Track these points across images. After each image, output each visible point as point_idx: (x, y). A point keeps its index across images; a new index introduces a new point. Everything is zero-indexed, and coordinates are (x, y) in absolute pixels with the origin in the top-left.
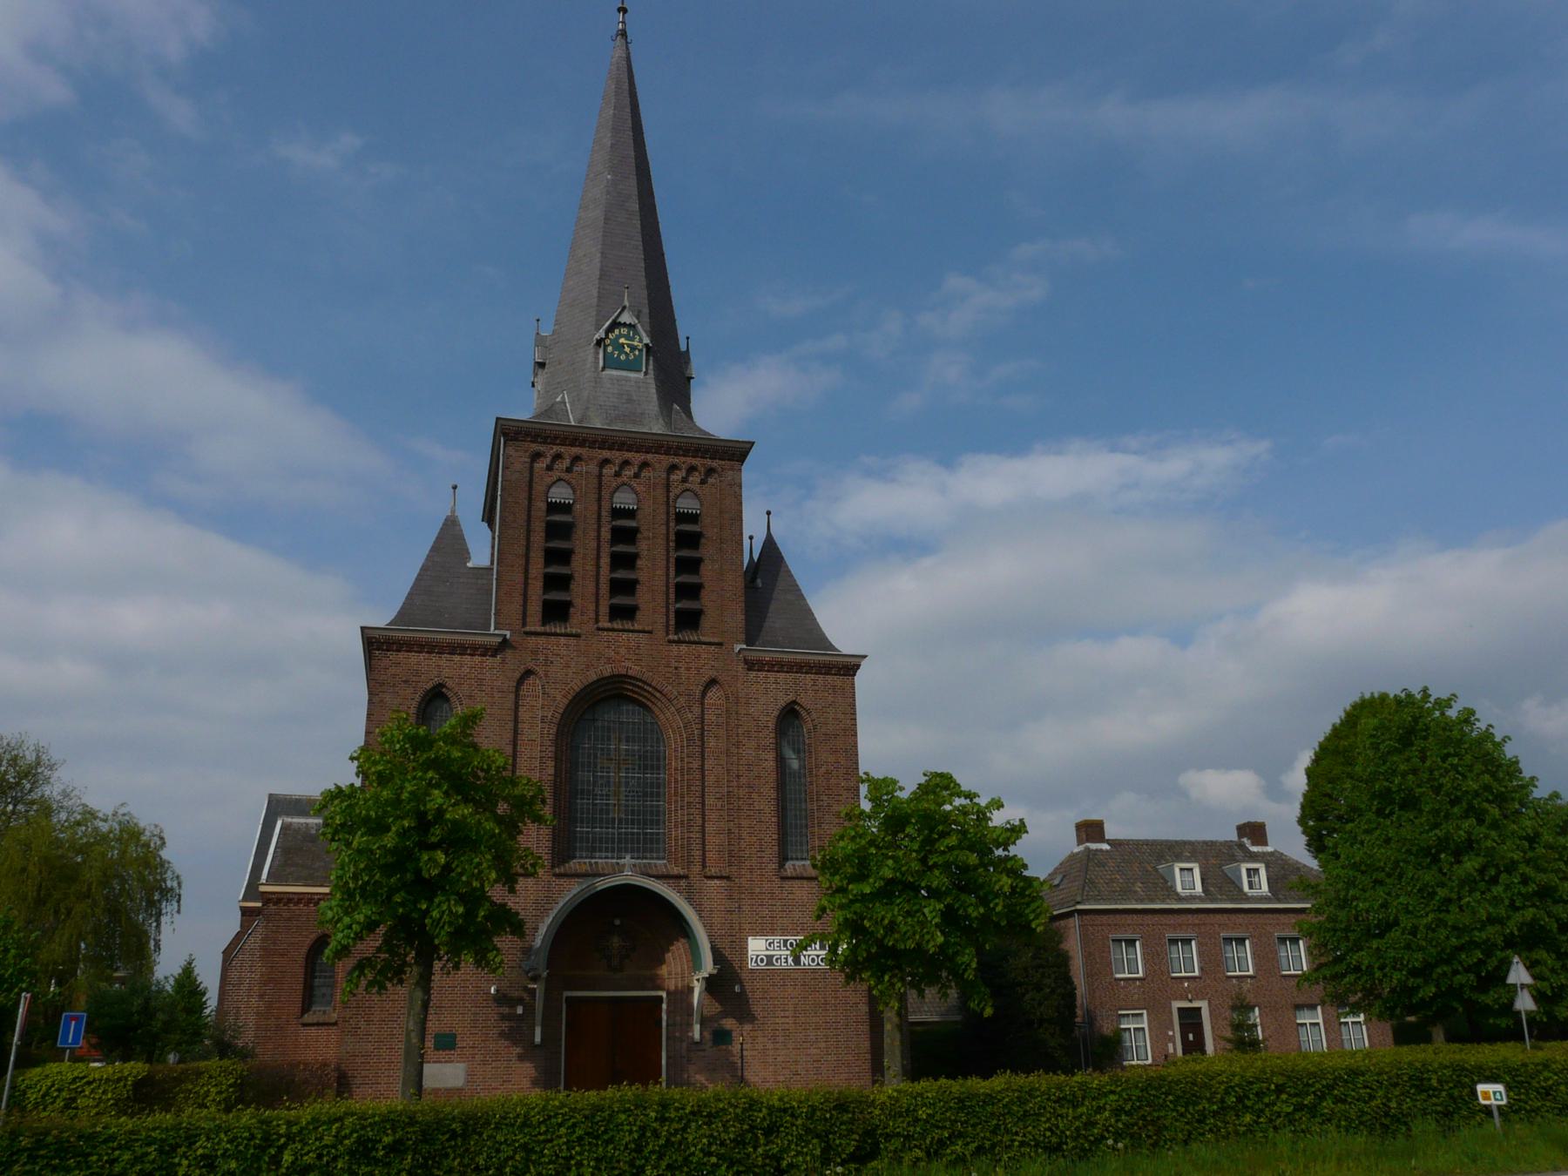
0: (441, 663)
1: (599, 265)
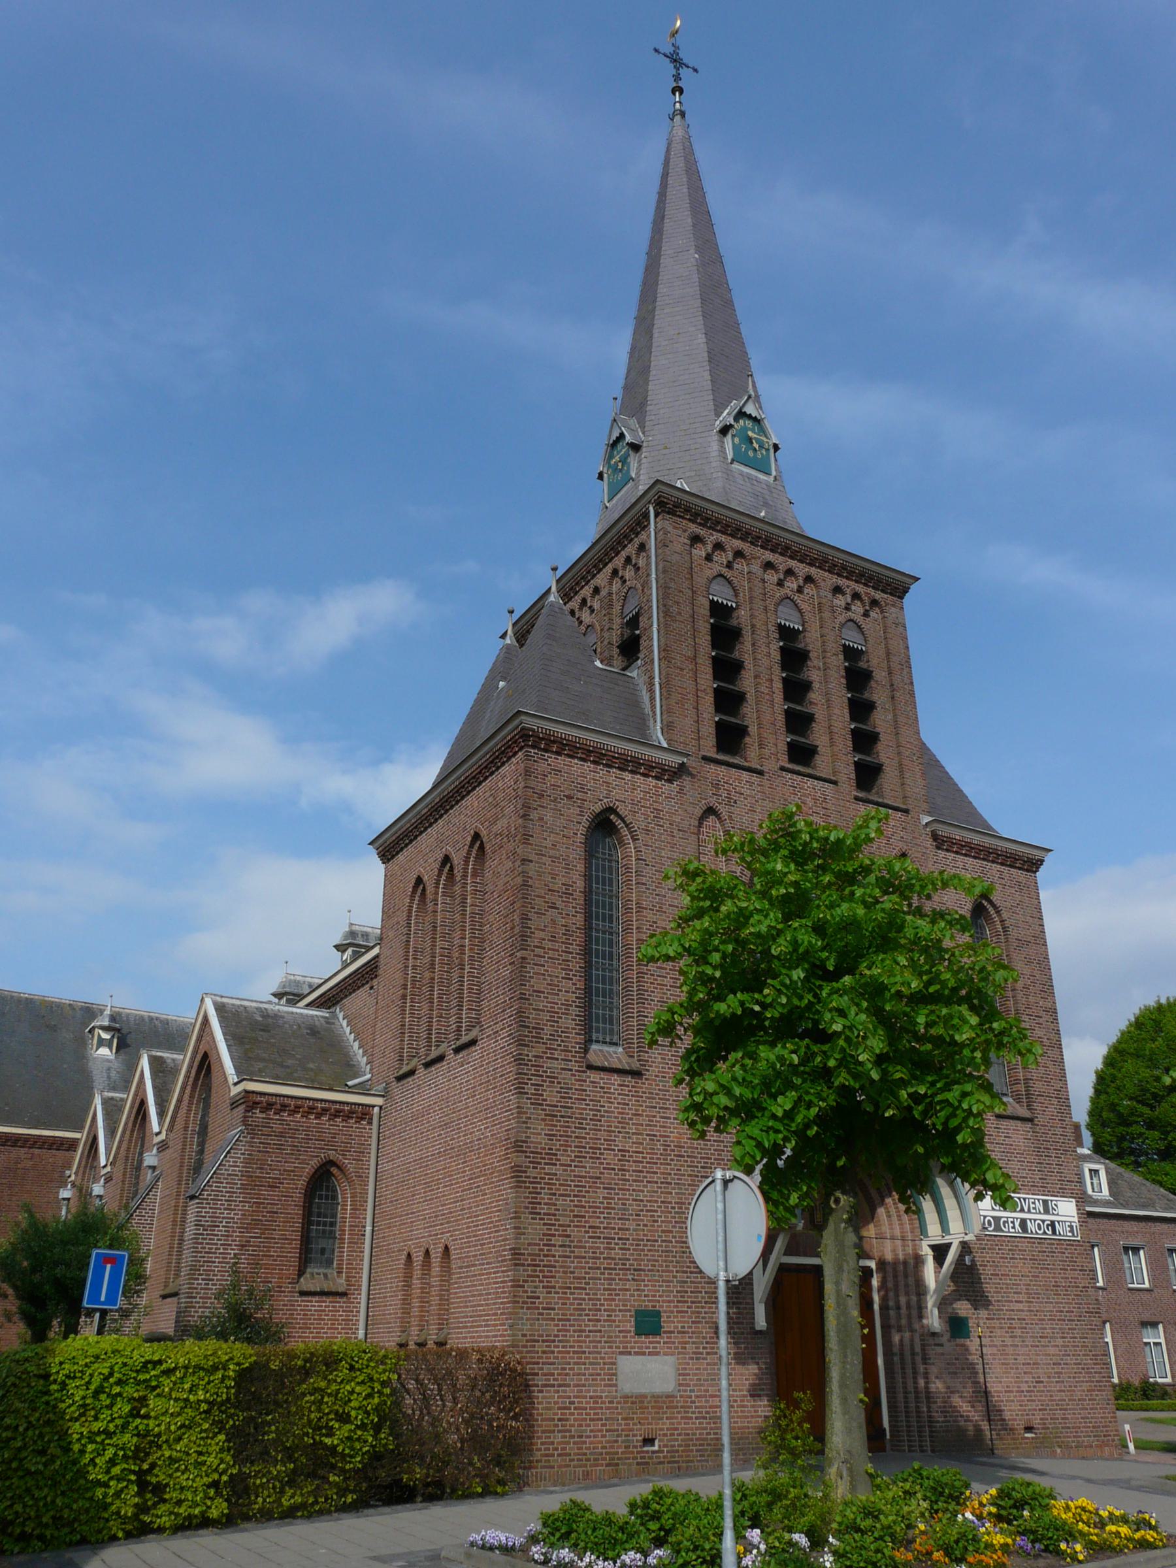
0: (610, 779)
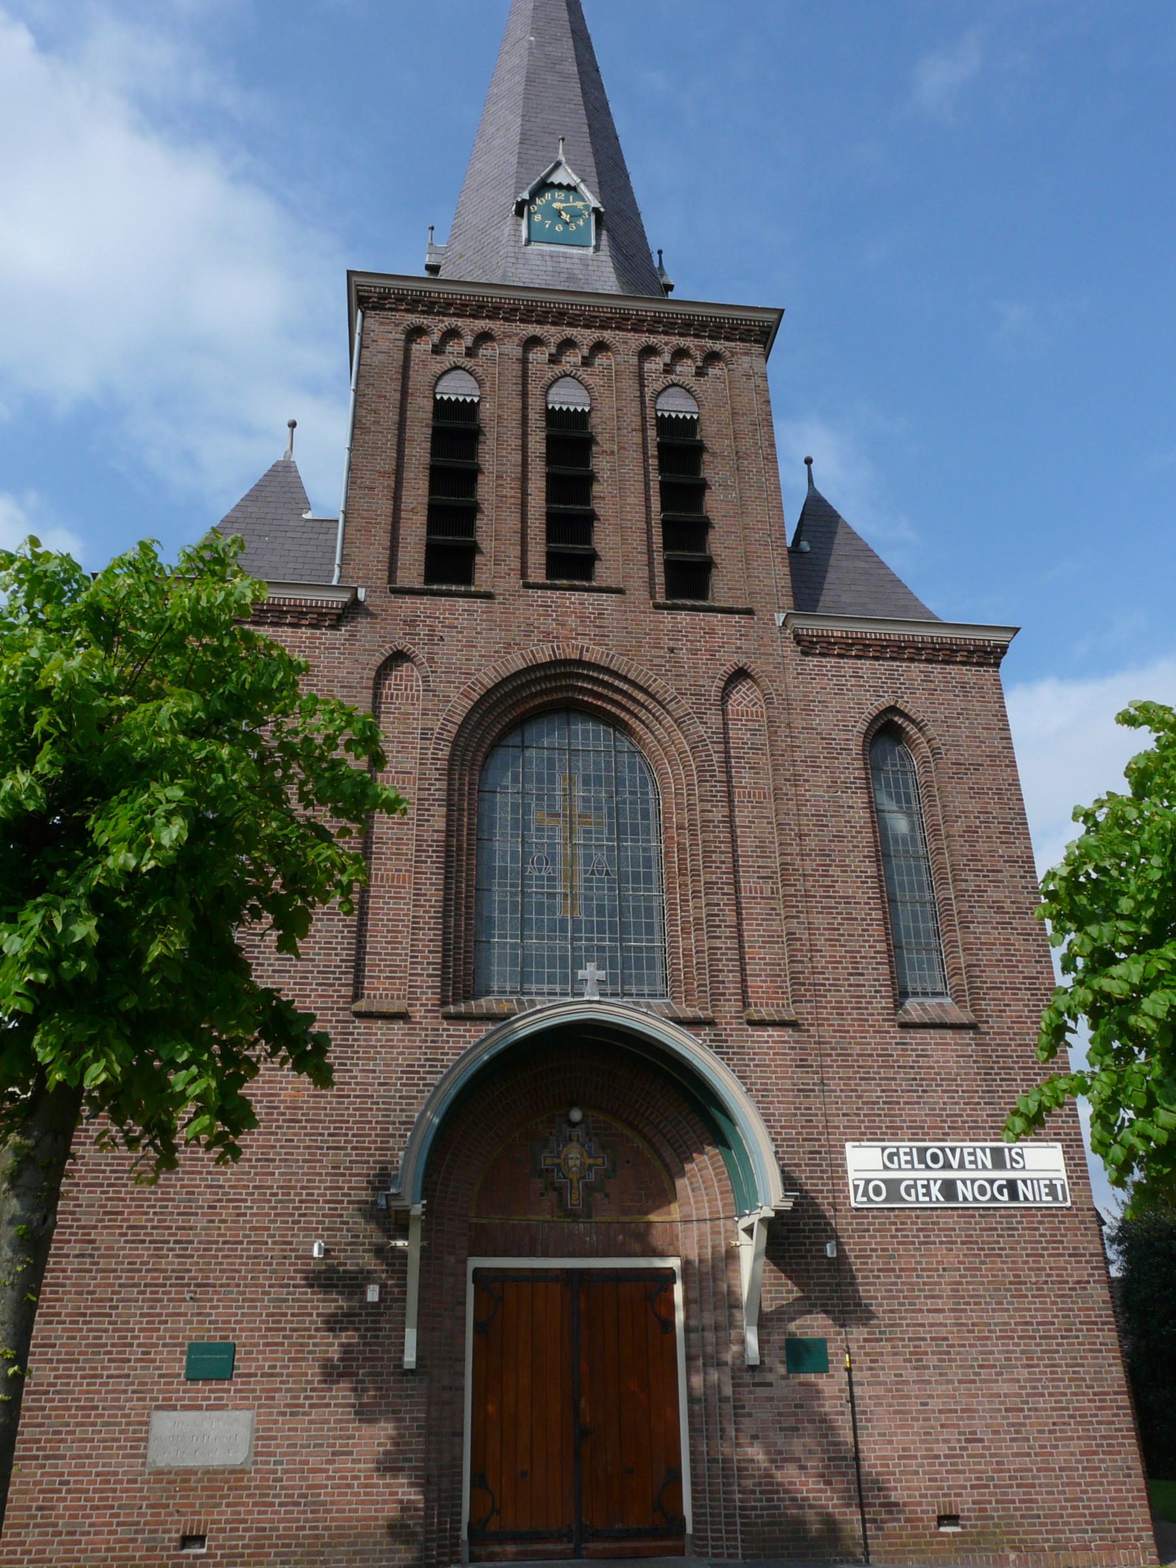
1: (519, 130)
